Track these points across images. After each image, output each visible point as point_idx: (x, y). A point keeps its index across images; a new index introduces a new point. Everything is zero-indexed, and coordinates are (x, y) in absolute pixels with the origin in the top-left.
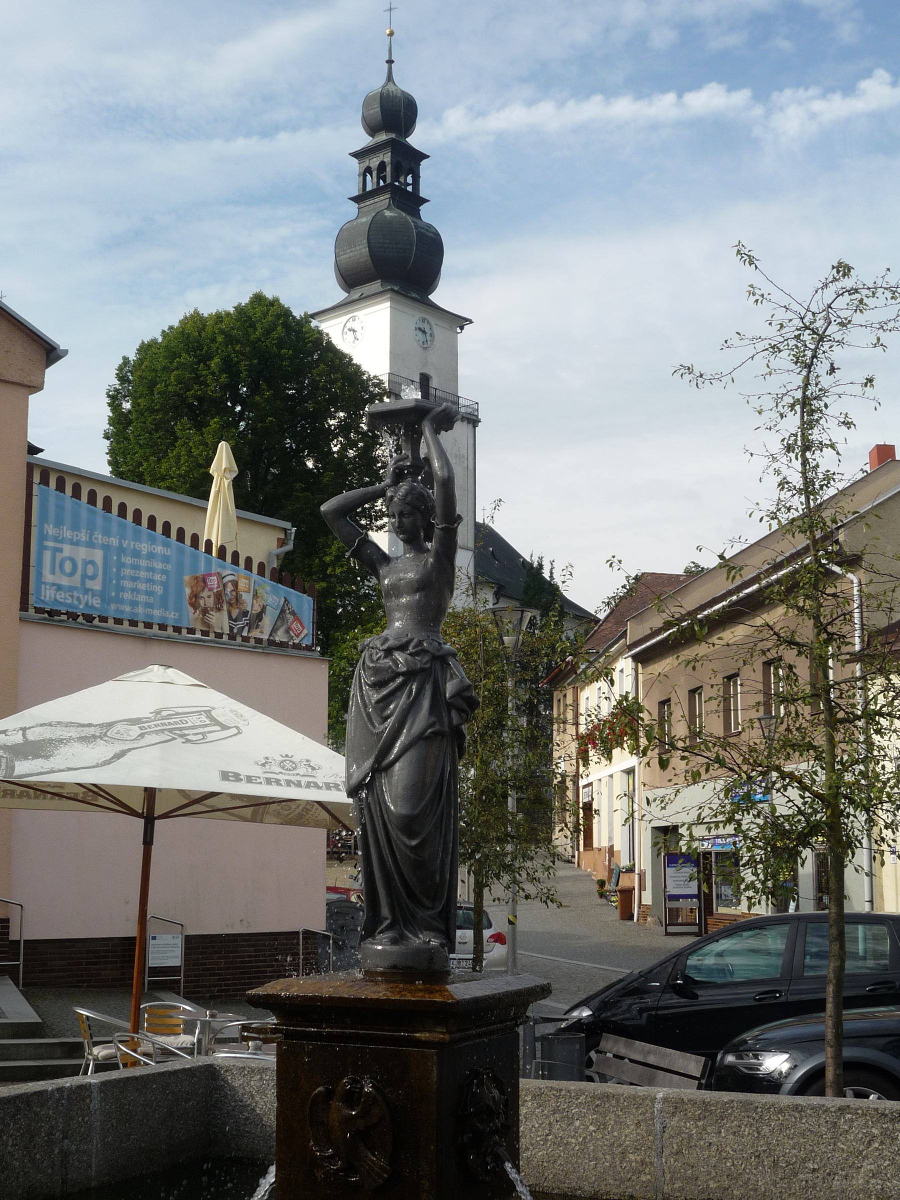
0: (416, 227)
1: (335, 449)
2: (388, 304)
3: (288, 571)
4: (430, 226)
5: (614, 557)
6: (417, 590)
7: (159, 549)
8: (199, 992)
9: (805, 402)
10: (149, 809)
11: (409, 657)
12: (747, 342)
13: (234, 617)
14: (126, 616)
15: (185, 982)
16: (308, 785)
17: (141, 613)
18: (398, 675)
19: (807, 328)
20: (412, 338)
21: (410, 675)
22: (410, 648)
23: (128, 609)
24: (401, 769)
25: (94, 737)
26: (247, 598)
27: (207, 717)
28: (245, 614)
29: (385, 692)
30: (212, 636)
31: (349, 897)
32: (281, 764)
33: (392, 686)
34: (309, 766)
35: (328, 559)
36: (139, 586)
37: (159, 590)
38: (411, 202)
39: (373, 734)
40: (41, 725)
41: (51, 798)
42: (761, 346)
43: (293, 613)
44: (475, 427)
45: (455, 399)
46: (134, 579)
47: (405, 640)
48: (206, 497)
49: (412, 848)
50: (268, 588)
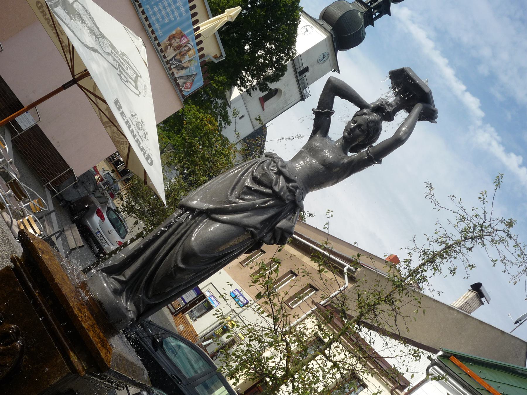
0: (361, 28)
1: (259, 53)
2: (326, 37)
3: (209, 68)
4: (365, 33)
5: (332, 212)
6: (324, 165)
7: (183, 10)
8: (18, 144)
9: (449, 247)
10: (79, 77)
11: (285, 188)
12: (459, 205)
13: (176, 58)
14: (147, 14)
15: (19, 137)
16: (137, 141)
17: (153, 19)
18: (271, 188)
19: (482, 226)
20: (318, 55)
21: (275, 195)
22: (290, 185)
23: (151, 13)
24: (218, 228)
25: (94, 33)
26: (187, 58)
27: (136, 77)
28: (180, 62)
29: (256, 187)
30: (162, 54)
31: (95, 175)
32: (138, 123)
33: (262, 189)
34: (145, 135)
35: (216, 78)
36: (163, 11)
37: (167, 20)
38: (369, 20)
39: (227, 197)
40: (83, 7)
41: (54, 33)
42: (461, 212)
43: (193, 81)
44: (301, 100)
45: (306, 86)
46: (164, 8)
47: (292, 178)
48: (213, 16)
49: (176, 266)
50: (196, 64)
